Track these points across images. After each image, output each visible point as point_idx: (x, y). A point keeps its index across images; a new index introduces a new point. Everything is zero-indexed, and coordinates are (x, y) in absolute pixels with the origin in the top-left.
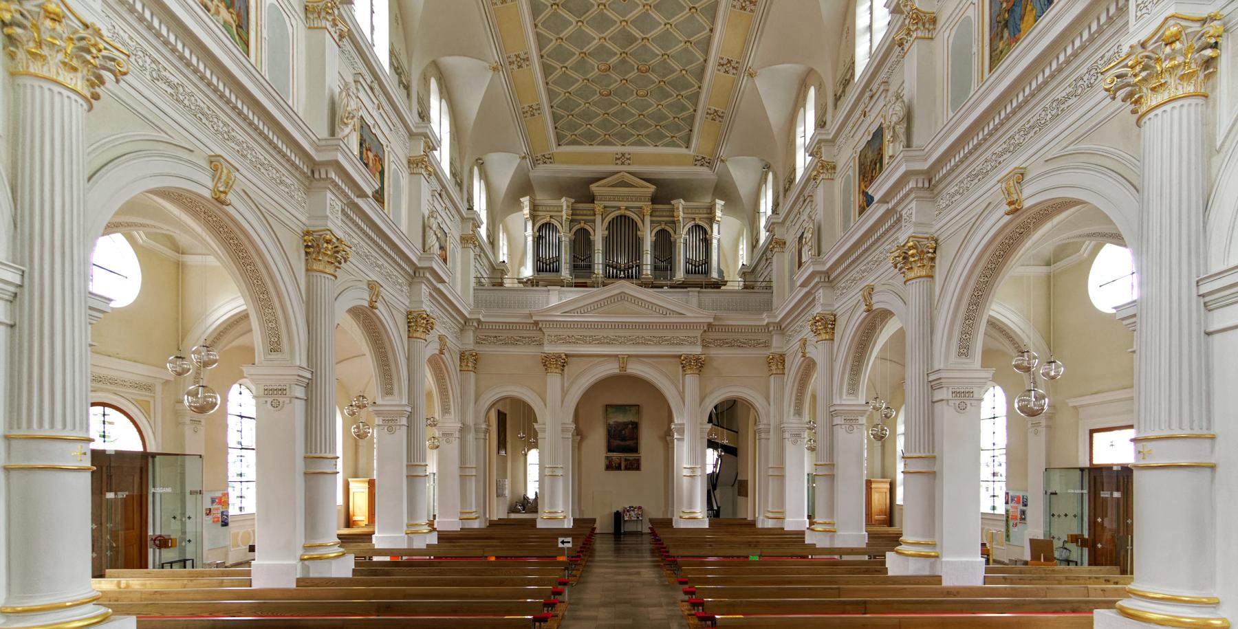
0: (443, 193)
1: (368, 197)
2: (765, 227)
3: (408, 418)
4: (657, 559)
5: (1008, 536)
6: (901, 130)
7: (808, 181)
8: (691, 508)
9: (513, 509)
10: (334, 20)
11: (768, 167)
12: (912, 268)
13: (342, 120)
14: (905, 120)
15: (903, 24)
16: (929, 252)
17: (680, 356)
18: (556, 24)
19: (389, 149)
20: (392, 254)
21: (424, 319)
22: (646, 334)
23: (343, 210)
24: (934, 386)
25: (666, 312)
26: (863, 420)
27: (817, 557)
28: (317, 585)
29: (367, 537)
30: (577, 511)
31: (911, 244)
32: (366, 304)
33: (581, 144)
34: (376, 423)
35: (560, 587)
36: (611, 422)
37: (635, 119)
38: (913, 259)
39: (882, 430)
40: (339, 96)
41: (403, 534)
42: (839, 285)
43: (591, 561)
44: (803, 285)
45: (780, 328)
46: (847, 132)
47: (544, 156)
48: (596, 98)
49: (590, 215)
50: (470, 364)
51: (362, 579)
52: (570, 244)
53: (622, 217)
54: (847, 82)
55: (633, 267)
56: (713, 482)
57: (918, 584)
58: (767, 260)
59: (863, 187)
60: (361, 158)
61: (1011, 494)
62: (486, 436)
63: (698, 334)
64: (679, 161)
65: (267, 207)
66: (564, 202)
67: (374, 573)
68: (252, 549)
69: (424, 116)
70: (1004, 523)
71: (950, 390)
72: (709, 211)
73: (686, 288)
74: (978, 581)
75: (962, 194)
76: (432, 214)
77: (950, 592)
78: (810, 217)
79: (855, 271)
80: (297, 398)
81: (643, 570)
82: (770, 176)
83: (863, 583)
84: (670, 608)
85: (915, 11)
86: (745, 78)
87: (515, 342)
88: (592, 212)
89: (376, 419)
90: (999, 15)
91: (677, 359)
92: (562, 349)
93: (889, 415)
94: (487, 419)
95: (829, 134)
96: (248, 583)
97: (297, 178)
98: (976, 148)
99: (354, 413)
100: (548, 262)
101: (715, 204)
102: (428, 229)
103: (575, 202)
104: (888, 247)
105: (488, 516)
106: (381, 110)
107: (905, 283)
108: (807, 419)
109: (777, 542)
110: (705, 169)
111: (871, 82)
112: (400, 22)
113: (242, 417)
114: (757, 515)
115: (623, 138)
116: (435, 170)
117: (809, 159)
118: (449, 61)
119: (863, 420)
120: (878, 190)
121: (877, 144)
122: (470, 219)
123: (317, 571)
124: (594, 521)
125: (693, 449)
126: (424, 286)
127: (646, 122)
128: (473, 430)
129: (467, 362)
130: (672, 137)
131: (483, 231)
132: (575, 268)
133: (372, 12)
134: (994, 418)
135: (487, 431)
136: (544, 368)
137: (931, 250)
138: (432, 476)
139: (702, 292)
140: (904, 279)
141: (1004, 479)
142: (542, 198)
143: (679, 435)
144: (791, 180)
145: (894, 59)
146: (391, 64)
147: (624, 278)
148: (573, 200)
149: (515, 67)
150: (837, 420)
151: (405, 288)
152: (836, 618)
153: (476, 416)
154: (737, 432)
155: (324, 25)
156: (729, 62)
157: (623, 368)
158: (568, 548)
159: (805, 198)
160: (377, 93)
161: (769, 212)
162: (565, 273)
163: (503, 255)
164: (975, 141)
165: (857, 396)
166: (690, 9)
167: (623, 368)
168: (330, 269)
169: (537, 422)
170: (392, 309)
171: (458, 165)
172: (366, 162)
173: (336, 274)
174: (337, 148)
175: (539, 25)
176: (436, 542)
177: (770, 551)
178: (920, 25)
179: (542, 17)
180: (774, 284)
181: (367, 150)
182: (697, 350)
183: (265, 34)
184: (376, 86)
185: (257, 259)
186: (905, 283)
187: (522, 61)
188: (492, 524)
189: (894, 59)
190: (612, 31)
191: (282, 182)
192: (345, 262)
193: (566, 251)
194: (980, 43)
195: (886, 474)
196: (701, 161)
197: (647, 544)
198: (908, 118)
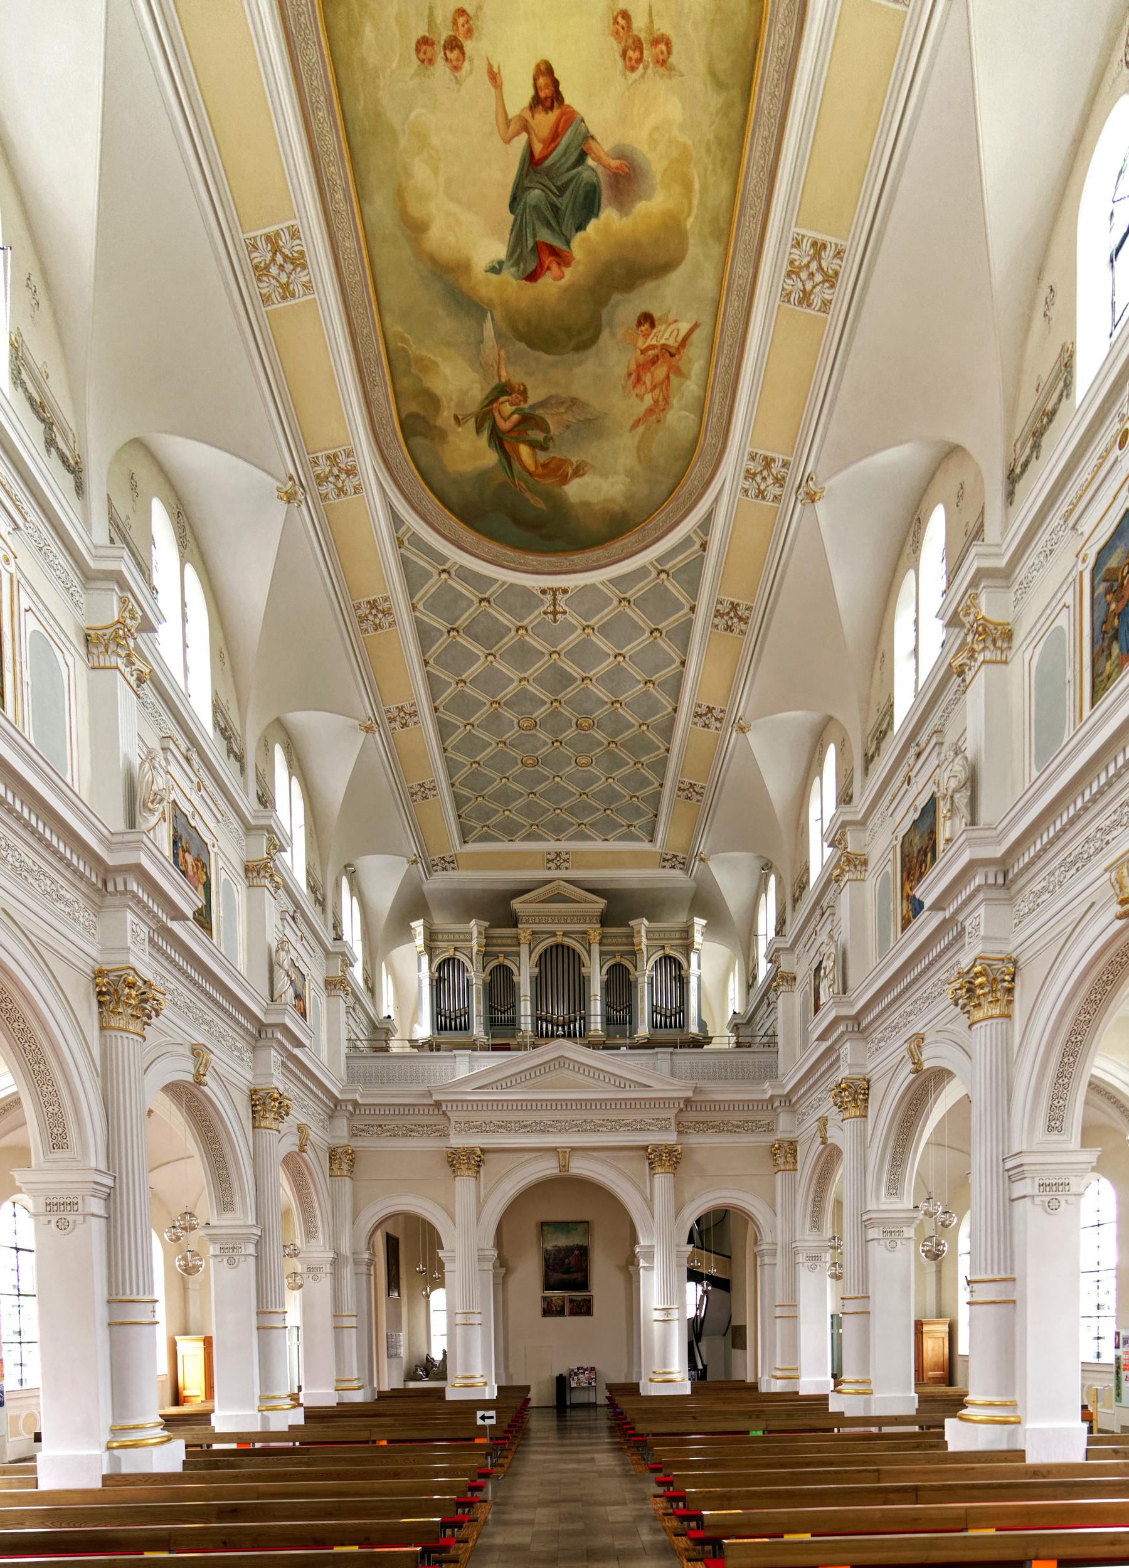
0: (298, 915)
1: (185, 918)
2: (766, 956)
3: (256, 1245)
4: (619, 1440)
5: (1118, 1395)
6: (962, 799)
7: (828, 882)
8: (665, 1367)
9: (411, 1376)
10: (128, 655)
11: (768, 866)
12: (979, 1004)
13: (145, 805)
14: (968, 785)
15: (964, 643)
16: (1005, 981)
17: (646, 1148)
18: (456, 659)
19: (216, 849)
20: (226, 1005)
21: (275, 1100)
22: (597, 1117)
23: (151, 940)
24: (1013, 1175)
25: (623, 1083)
26: (909, 1232)
27: (847, 1430)
28: (133, 1484)
29: (203, 1418)
30: (503, 1376)
31: (978, 969)
32: (190, 1079)
33: (497, 840)
34: (212, 1252)
35: (479, 1480)
36: (549, 1246)
37: (573, 800)
38: (982, 992)
39: (938, 1244)
40: (140, 768)
41: (255, 1412)
42: (874, 1036)
43: (523, 1445)
44: (821, 1038)
45: (789, 1101)
46: (883, 808)
47: (443, 859)
48: (517, 769)
49: (514, 946)
50: (345, 1167)
51: (198, 1474)
52: (484, 989)
53: (558, 949)
54: (881, 734)
55: (575, 1020)
56: (696, 1330)
57: (991, 1461)
58: (769, 1004)
59: (907, 887)
60: (176, 862)
61: (1123, 1333)
62: (369, 1270)
63: (671, 1114)
64: (639, 860)
65: (39, 935)
66: (474, 926)
67: (215, 1465)
68: (38, 1438)
69: (265, 800)
70: (1113, 1377)
71: (1037, 1179)
72: (684, 935)
73: (653, 1048)
74: (1078, 1457)
75: (1052, 892)
76: (283, 944)
77: (1038, 1471)
78: (831, 937)
79: (897, 1014)
80: (93, 1215)
81: (596, 1456)
82: (772, 880)
83: (913, 1462)
84: (638, 1506)
85: (981, 621)
86: (734, 734)
87: (409, 1133)
88: (515, 942)
89: (211, 1248)
90: (1105, 622)
91: (642, 1153)
92: (477, 1141)
93: (947, 1222)
94: (371, 1246)
95: (856, 813)
96: (34, 1482)
97: (81, 891)
98: (1072, 822)
99: (178, 1238)
100: (453, 1016)
101: (693, 924)
102: (276, 968)
103: (491, 927)
104: (944, 977)
105: (375, 1385)
106: (203, 792)
107: (970, 1026)
108: (830, 1235)
109: (789, 1410)
110: (677, 873)
111: (918, 734)
112: (226, 660)
113: (18, 1249)
114: (759, 1376)
115: (558, 830)
116: (284, 880)
117: (828, 851)
118: (300, 719)
119: (909, 1232)
120: (929, 890)
121: (927, 822)
122: (337, 953)
123: (134, 1463)
124: (527, 1389)
125: (666, 1281)
126: (273, 1052)
127: (591, 805)
128: (351, 1260)
129: (340, 1164)
130: (629, 826)
131: (357, 972)
132: (492, 1023)
133: (186, 646)
134: (1099, 1225)
135: (371, 1263)
136: (450, 1170)
137: (1007, 978)
138: (295, 1330)
139: (677, 1054)
140: (969, 1022)
141: (1113, 1312)
142: (441, 921)
143: (647, 1262)
144: (802, 885)
145: (951, 696)
146: (216, 724)
147: (563, 1036)
148: (487, 924)
149: (397, 725)
150: (873, 1233)
151: (247, 1056)
152: (875, 1510)
153: (355, 1238)
154: (729, 1257)
155: (114, 665)
156: (710, 710)
157: (564, 1167)
158: (491, 1426)
159: (822, 909)
160: (196, 767)
161: (772, 934)
162: (478, 1030)
163: (387, 1006)
164: (1072, 812)
165: (901, 1198)
166: (652, 633)
167: (564, 1167)
168: (135, 1026)
169: (443, 1248)
170: (226, 1084)
171: (318, 874)
172: (183, 868)
173: (145, 1033)
174: (138, 845)
175: (431, 662)
176: (302, 1422)
177: (778, 1422)
178: (989, 643)
179: (436, 649)
180: (780, 1040)
181: (184, 851)
182: (670, 1138)
183: (27, 677)
184: (194, 756)
185: (28, 1013)
186: (970, 1026)
187: (407, 717)
188: (382, 1396)
189: (951, 696)
190: (537, 668)
191: (60, 898)
192: (157, 1016)
193: (478, 998)
194: (1078, 666)
195: (943, 1311)
196: (669, 860)
197: (603, 1420)
198: (972, 781)
